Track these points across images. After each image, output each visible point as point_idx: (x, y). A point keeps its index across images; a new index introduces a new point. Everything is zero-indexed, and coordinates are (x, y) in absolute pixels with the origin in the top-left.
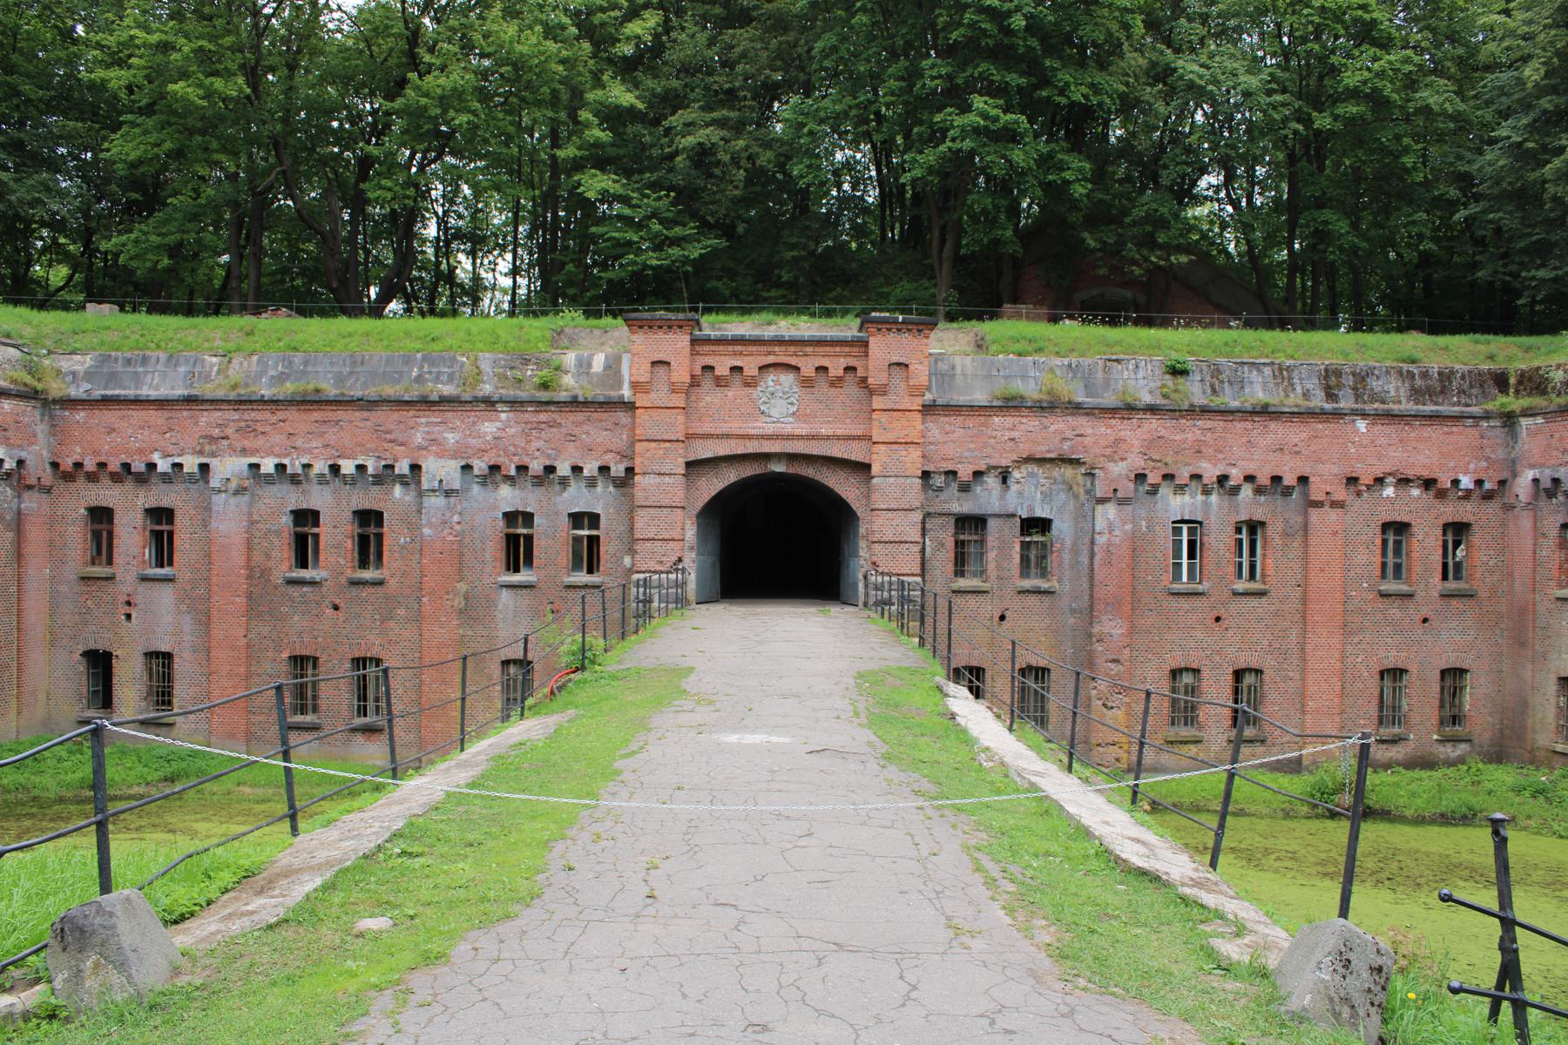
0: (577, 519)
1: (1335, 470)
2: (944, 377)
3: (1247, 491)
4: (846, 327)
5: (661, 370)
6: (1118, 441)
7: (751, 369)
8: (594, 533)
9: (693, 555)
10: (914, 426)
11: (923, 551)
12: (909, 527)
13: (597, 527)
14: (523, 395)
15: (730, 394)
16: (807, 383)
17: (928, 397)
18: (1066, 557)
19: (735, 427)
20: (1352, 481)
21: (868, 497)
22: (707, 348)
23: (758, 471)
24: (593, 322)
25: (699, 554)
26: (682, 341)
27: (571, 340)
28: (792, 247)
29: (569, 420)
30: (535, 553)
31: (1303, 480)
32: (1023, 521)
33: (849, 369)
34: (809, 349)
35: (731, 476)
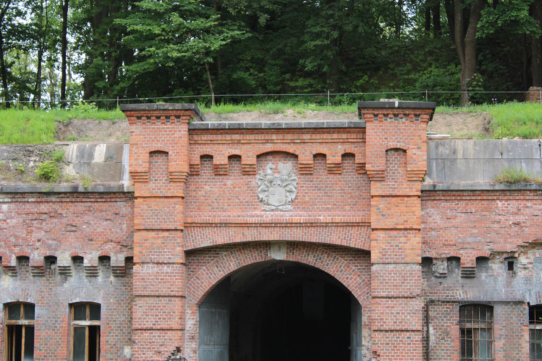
0: (78, 309)
2: (448, 162)
4: (345, 114)
5: (159, 160)
7: (249, 158)
8: (95, 323)
9: (194, 345)
10: (413, 212)
11: (426, 339)
12: (410, 315)
13: (98, 318)
14: (23, 186)
15: (229, 183)
16: (305, 170)
17: (428, 182)
19: (234, 215)
21: (369, 284)
22: (205, 137)
23: (259, 259)
24: (104, 113)
25: (202, 343)
26: (180, 130)
27: (80, 132)
28: (318, 36)
29: (70, 210)
30: (36, 345)
32: (532, 308)
33: (347, 156)
34: (307, 137)
35: (231, 264)
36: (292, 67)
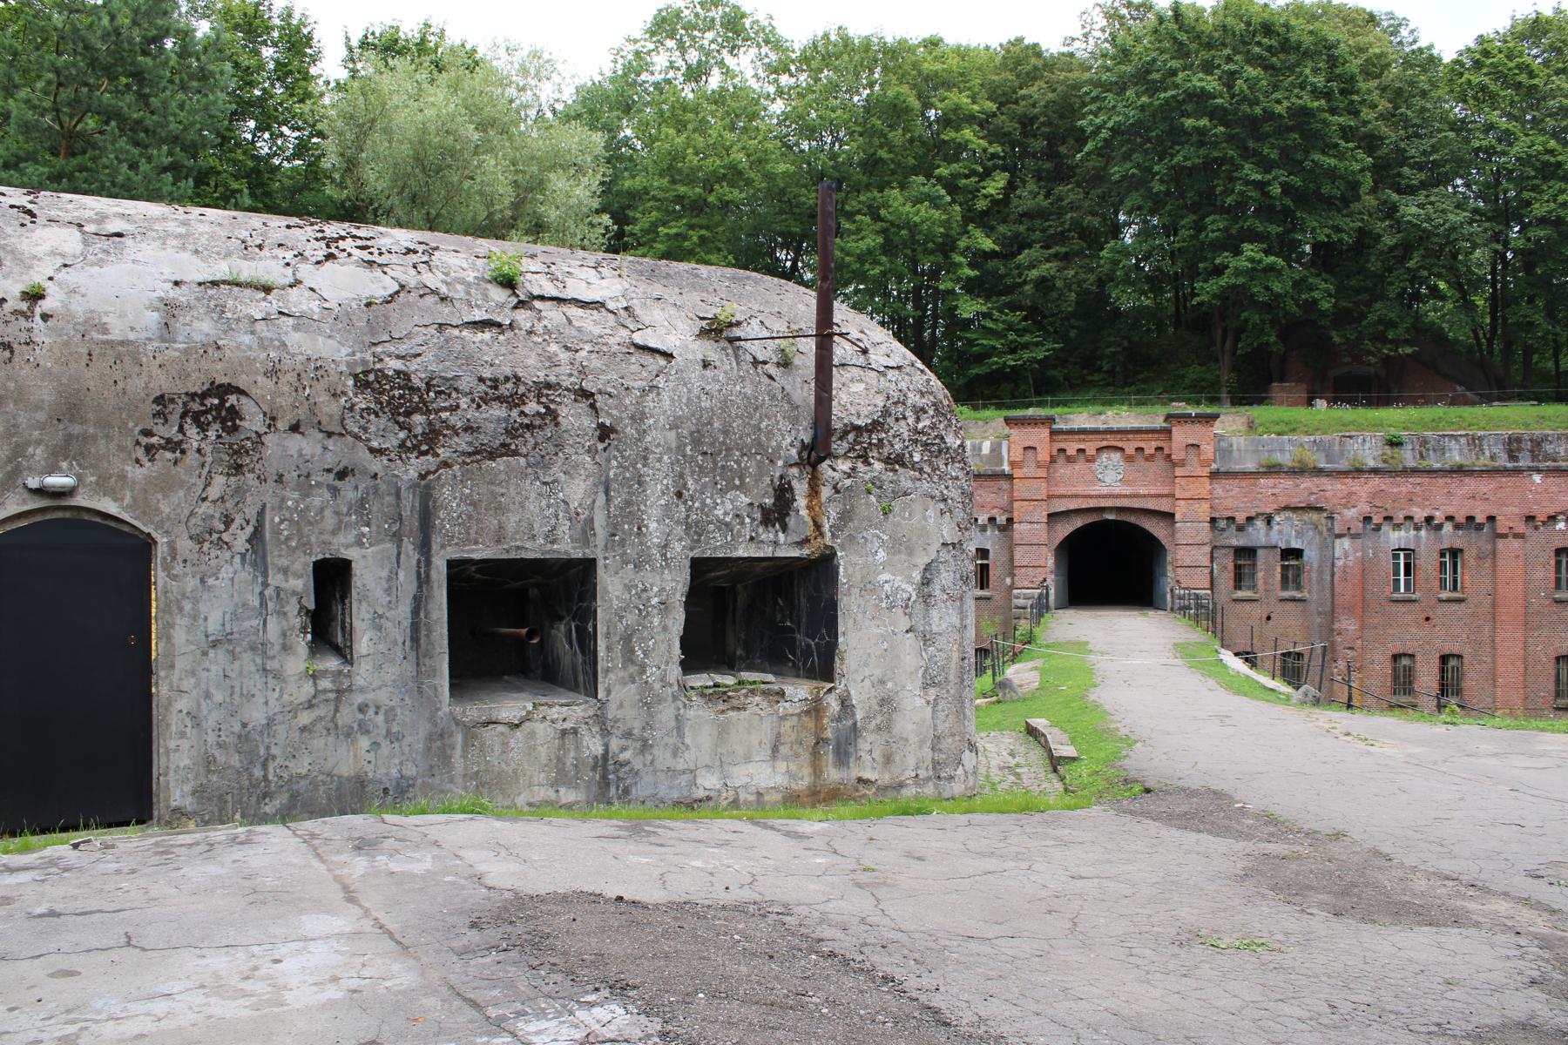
1: (1516, 511)
3: (1448, 527)
5: (1030, 453)
6: (1351, 494)
7: (1091, 451)
10: (1203, 488)
16: (1129, 459)
17: (1214, 466)
18: (1314, 575)
20: (1530, 519)
21: (1173, 535)
31: (1491, 519)
32: (1283, 551)
33: (1159, 449)
35: (1078, 523)
36: (1089, 363)
